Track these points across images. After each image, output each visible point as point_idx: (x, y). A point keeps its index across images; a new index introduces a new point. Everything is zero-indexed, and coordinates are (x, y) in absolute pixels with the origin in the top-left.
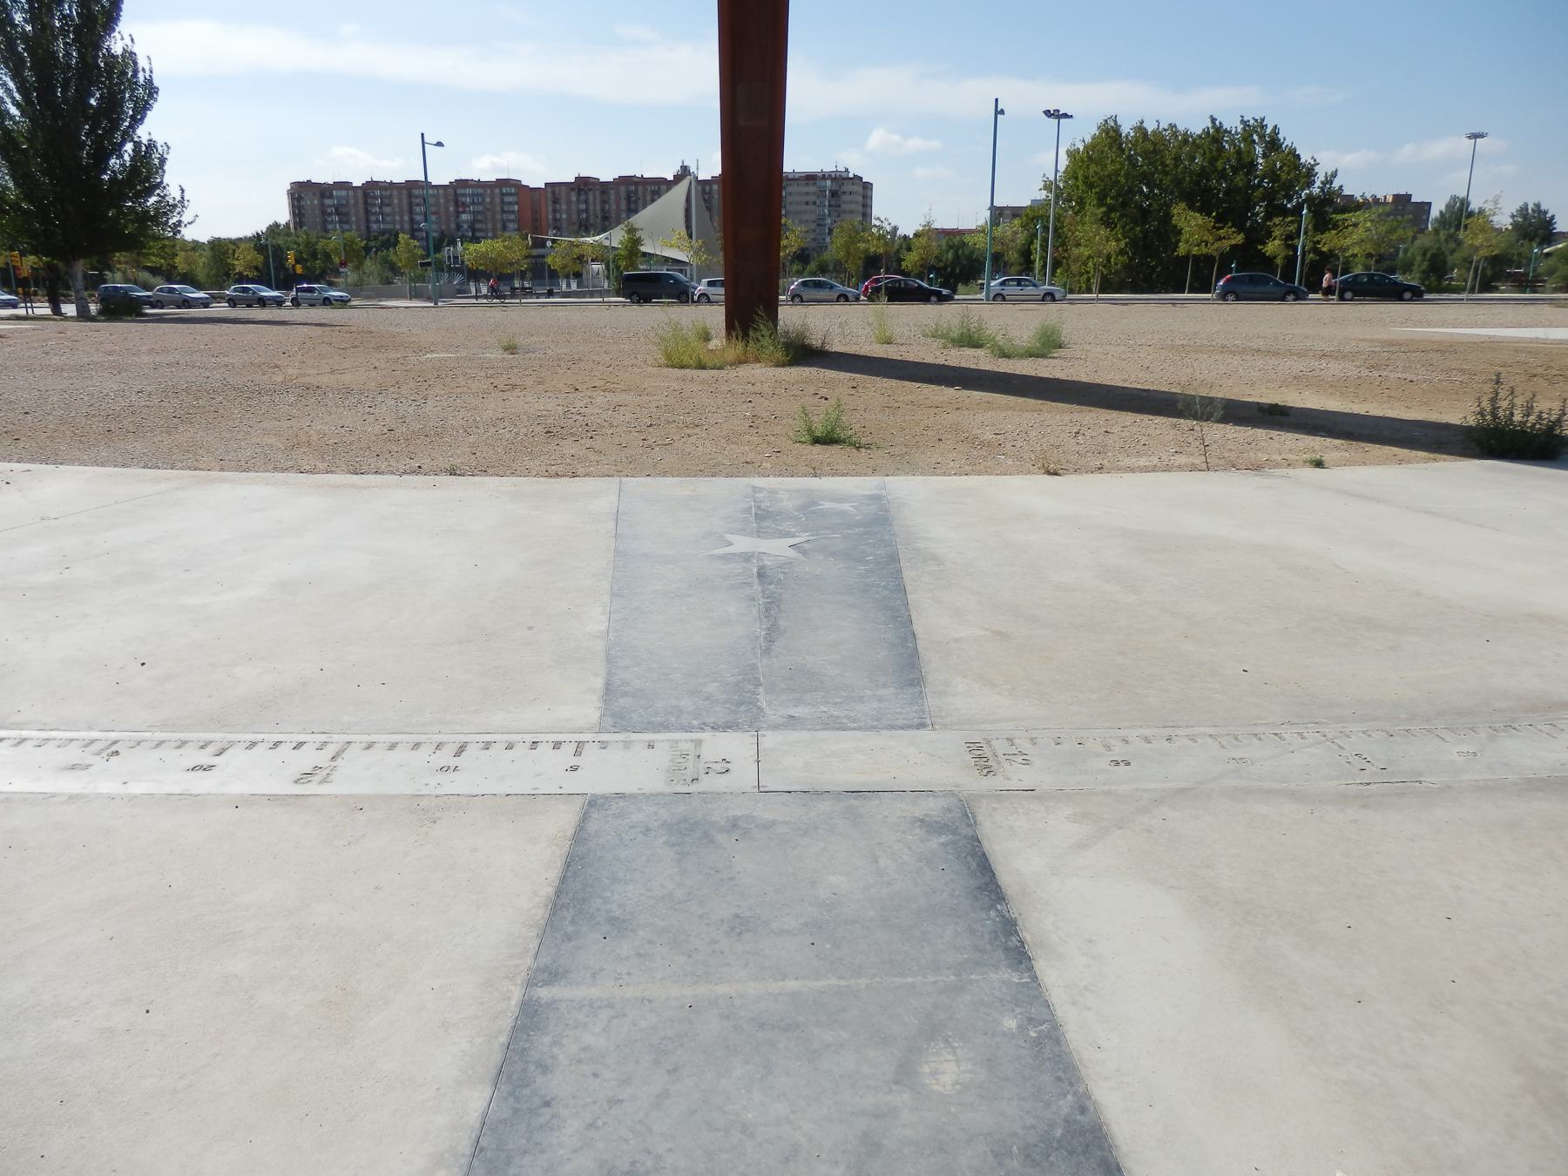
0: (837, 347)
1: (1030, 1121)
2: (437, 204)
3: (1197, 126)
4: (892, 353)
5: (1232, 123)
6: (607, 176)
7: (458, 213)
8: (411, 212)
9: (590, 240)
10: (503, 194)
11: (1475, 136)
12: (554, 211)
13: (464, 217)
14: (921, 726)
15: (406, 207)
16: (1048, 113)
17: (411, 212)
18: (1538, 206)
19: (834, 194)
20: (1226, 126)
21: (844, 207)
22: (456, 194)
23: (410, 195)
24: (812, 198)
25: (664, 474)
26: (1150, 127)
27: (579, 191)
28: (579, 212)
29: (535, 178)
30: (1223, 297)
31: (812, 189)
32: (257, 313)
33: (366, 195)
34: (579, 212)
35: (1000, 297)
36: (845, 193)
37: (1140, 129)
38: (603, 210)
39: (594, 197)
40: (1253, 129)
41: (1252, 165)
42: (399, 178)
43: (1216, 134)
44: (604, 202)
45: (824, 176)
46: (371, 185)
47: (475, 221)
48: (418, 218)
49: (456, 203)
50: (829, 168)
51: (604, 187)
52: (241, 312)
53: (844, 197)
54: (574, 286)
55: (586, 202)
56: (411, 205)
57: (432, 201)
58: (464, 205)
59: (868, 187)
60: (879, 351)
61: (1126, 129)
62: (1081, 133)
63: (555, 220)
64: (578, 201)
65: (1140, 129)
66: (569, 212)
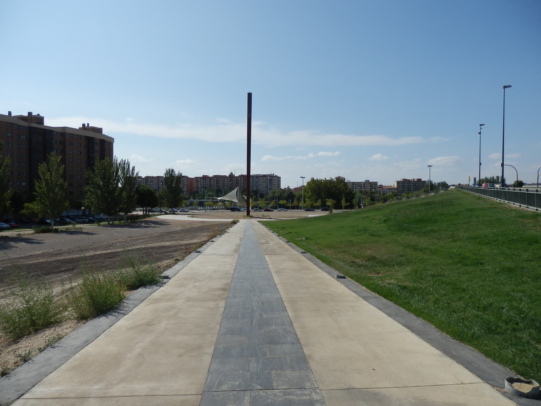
1: (126, 309)
6: (211, 175)
8: (158, 184)
9: (219, 198)
14: (60, 339)
17: (158, 184)
19: (270, 180)
23: (158, 180)
25: (264, 176)
26: (315, 179)
27: (204, 179)
31: (264, 179)
32: (185, 213)
33: (146, 180)
39: (208, 181)
41: (30, 202)
42: (155, 175)
44: (210, 182)
45: (268, 176)
46: (215, 176)
51: (210, 178)
56: (158, 182)
59: (279, 178)
66: (201, 184)
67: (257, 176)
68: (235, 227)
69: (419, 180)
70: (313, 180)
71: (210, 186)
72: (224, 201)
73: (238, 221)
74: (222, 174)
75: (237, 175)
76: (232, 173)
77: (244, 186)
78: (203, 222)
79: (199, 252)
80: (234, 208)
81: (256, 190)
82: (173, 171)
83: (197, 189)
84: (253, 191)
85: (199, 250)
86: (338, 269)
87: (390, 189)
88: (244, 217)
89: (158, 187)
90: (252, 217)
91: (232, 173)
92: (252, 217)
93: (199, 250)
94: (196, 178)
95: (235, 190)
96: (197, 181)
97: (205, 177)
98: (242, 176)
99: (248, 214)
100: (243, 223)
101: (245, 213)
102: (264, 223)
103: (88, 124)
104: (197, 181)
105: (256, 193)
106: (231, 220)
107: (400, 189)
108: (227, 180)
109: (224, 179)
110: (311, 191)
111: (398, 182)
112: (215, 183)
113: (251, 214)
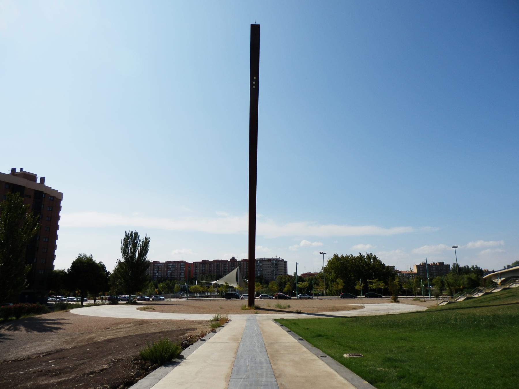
0: (262, 307)
2: (161, 268)
3: (356, 255)
4: (270, 308)
5: (364, 254)
6: (211, 260)
7: (167, 270)
8: (154, 270)
9: (213, 282)
10: (181, 265)
11: (455, 247)
12: (195, 270)
13: (169, 271)
15: (152, 269)
16: (321, 253)
18: (476, 266)
19: (276, 264)
20: (363, 255)
21: (279, 268)
22: (167, 265)
23: (154, 265)
24: (270, 266)
25: (269, 260)
28: (203, 270)
29: (190, 261)
30: (341, 298)
32: (160, 302)
34: (203, 270)
35: (300, 298)
36: (279, 265)
37: (342, 256)
38: (209, 269)
40: (369, 256)
43: (361, 257)
44: (210, 267)
45: (273, 260)
47: (172, 273)
48: (156, 272)
49: (167, 268)
50: (274, 257)
52: (157, 302)
53: (279, 265)
54: (209, 294)
55: (205, 267)
56: (154, 268)
57: (160, 267)
58: (169, 268)
59: (286, 262)
60: (268, 308)
61: (340, 256)
62: (330, 256)
63: (195, 272)
64: (202, 267)
65: (342, 256)
66: (199, 270)
67: (262, 261)
68: (223, 333)
69: (442, 264)
70: (336, 256)
71: (210, 272)
72: (217, 286)
73: (227, 321)
74: (223, 258)
75: (239, 259)
76: (233, 258)
77: (247, 272)
78: (142, 323)
79: (204, 340)
80: (230, 295)
81: (260, 276)
82: (136, 234)
83: (196, 275)
84: (258, 277)
85: (203, 338)
86: (299, 335)
87: (409, 274)
88: (244, 310)
89: (153, 273)
90: (258, 308)
91: (233, 258)
92: (258, 308)
93: (203, 338)
94: (195, 263)
95: (235, 271)
96: (196, 267)
97: (204, 262)
98: (245, 260)
99: (251, 303)
100: (239, 322)
101: (246, 302)
102: (282, 323)
103: (43, 179)
104: (196, 267)
105: (259, 280)
106: (210, 317)
107: (421, 274)
108: (229, 264)
109: (225, 264)
110: (335, 272)
111: (418, 266)
112: (215, 268)
113: (258, 302)
